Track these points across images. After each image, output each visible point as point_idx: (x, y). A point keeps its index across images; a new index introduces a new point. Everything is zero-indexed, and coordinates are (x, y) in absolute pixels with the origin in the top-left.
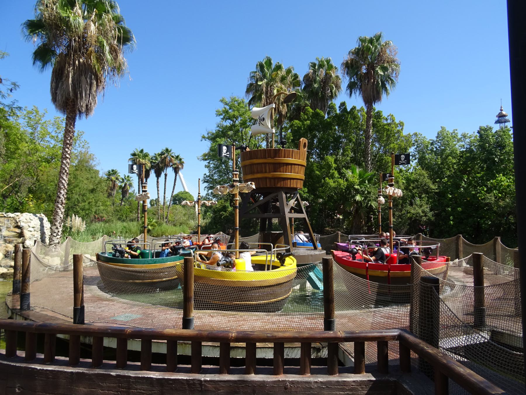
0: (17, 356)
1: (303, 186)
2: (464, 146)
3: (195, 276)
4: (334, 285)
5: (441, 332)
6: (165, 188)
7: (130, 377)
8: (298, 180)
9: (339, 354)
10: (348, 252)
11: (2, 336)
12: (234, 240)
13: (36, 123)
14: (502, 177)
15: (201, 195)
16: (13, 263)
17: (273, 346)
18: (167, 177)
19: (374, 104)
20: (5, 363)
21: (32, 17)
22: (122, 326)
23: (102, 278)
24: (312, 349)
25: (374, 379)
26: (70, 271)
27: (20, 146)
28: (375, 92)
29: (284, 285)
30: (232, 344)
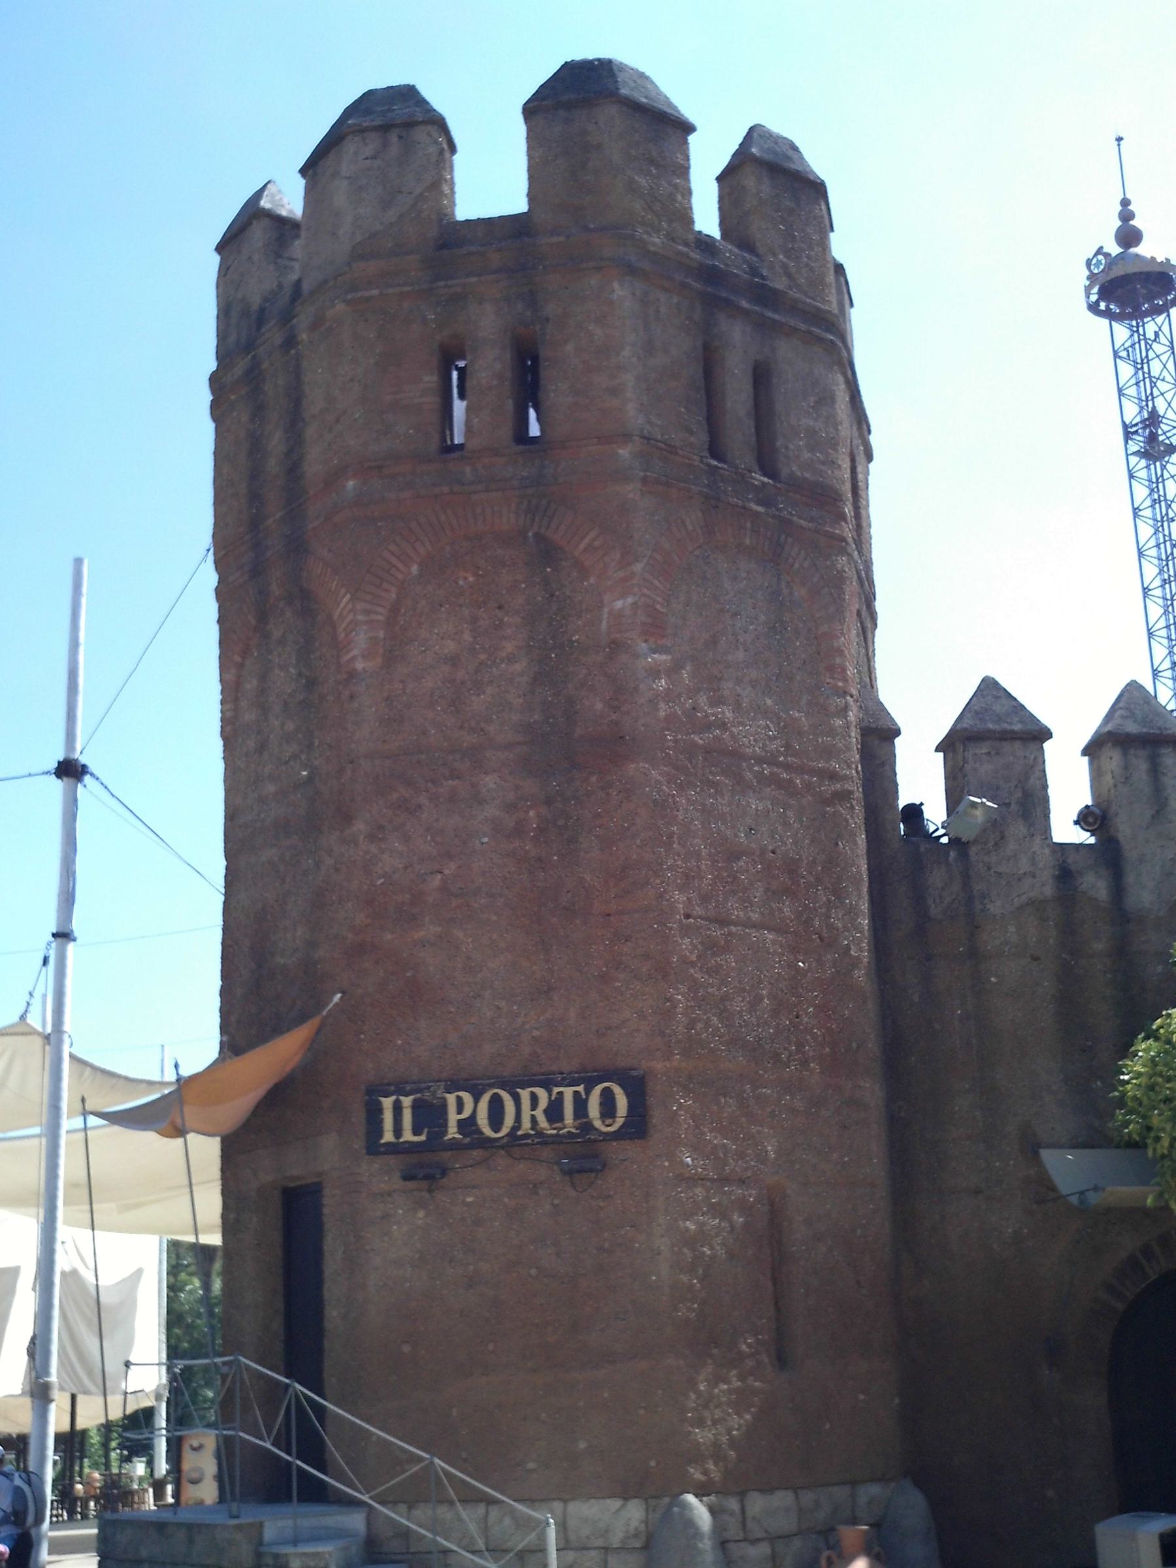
0: (529, 210)
1: (493, 1130)
2: (587, 852)
3: (63, 1274)
4: (777, 287)
5: (95, 1544)
6: (1137, 537)
7: (869, 869)
8: (194, 1181)
9: (592, 1093)
10: (392, 1095)
11: (706, 1472)
12: (864, 423)
13: (310, 746)
14: (817, 269)
15: (89, 776)
16: (104, 1461)
17: (456, 442)
18: (109, 787)
19: (1170, 729)
20: (340, 1412)
21: (55, 932)
22: (47, 1067)
23: (452, 223)
24: (634, 1513)
25: (1092, 840)
26: (138, 1402)
27: (988, 907)
28: (275, 386)
29: (114, 1081)
30: (1158, 464)
